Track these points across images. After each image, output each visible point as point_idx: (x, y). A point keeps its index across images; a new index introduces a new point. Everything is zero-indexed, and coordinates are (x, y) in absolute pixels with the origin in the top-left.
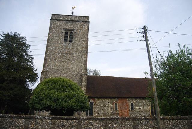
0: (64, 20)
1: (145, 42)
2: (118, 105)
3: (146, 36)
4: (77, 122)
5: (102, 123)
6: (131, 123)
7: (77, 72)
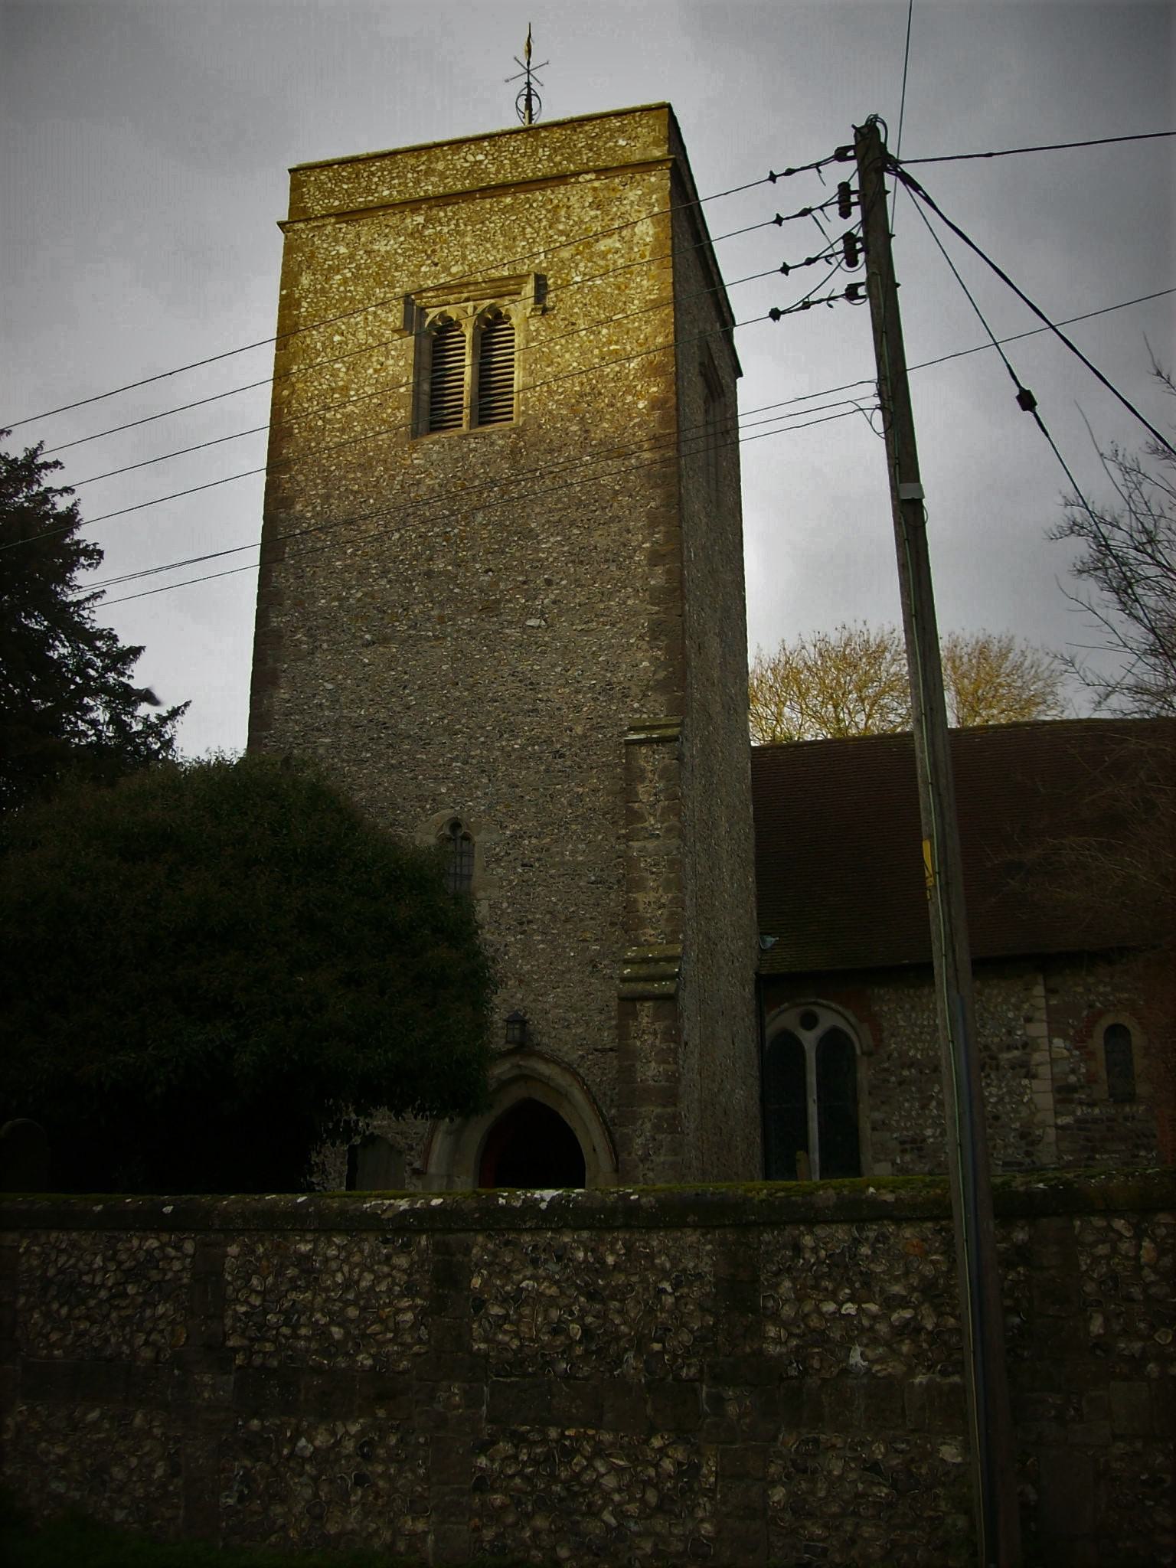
0: (413, 205)
1: (861, 313)
2: (1137, 1039)
3: (871, 246)
4: (189, 1247)
5: (402, 1261)
6: (698, 1252)
7: (579, 730)
